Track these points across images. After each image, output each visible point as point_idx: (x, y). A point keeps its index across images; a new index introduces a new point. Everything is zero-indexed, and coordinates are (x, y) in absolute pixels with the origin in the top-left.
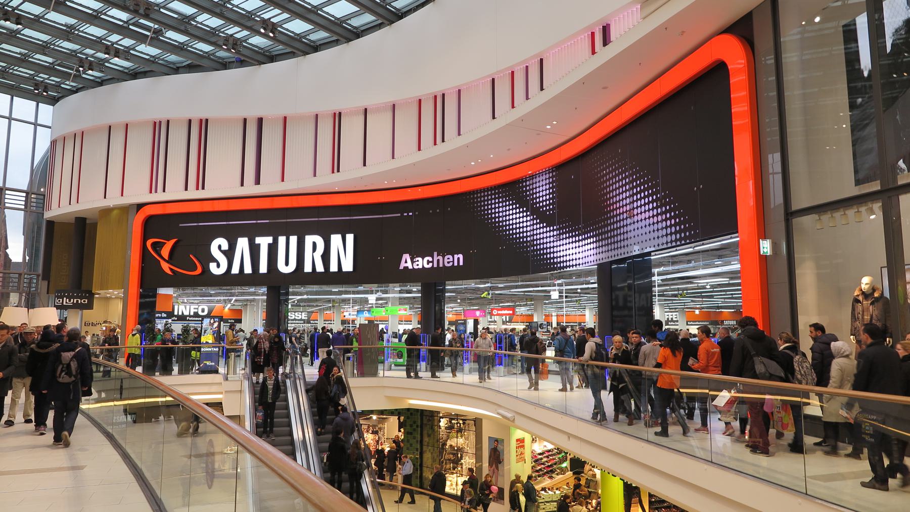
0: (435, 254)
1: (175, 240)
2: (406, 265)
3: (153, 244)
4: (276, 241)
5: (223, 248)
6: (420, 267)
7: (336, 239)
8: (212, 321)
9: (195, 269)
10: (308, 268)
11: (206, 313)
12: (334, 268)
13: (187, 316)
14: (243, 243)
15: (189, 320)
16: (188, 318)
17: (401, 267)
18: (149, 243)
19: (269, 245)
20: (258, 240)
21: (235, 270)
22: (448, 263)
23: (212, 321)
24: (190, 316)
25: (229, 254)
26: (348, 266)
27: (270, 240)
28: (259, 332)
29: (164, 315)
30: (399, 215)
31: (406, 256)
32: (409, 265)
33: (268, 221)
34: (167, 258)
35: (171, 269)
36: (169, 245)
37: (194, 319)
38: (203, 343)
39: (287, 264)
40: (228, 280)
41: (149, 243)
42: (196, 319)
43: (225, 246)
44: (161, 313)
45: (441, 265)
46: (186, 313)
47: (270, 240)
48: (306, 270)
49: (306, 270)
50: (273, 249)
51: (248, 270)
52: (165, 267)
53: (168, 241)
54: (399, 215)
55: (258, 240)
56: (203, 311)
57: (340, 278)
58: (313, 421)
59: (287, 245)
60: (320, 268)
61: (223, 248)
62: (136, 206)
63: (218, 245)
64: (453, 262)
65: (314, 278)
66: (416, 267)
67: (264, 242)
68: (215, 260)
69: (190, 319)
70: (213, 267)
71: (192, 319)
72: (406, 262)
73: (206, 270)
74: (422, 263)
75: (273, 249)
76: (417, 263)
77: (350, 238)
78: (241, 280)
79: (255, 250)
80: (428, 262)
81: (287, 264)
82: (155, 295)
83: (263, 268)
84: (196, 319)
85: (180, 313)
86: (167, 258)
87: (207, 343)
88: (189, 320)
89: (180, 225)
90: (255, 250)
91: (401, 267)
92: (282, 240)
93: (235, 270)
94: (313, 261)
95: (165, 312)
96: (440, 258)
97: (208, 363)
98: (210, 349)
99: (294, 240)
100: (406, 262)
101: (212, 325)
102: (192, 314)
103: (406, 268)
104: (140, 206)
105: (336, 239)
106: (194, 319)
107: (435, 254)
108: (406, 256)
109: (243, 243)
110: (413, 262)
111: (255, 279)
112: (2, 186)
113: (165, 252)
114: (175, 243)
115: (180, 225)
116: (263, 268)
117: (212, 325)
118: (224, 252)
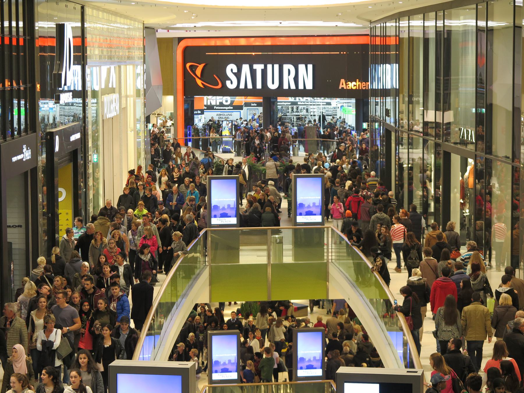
0: (357, 80)
1: (204, 64)
2: (343, 86)
3: (191, 67)
4: (266, 67)
5: (234, 71)
6: (350, 88)
7: (302, 67)
8: (228, 122)
9: (218, 85)
10: (286, 87)
11: (229, 103)
12: (301, 87)
13: (214, 106)
14: (246, 68)
15: (216, 109)
16: (215, 107)
17: (340, 88)
18: (188, 65)
19: (262, 70)
20: (255, 66)
21: (242, 86)
22: (364, 87)
23: (228, 122)
24: (217, 106)
25: (238, 75)
26: (309, 86)
27: (262, 66)
28: (8, 359)
29: (199, 112)
30: (338, 53)
31: (343, 81)
32: (344, 86)
33: (261, 53)
34: (199, 76)
35: (202, 84)
36: (201, 67)
37: (220, 108)
38: (224, 136)
39: (273, 83)
40: (237, 92)
41: (188, 65)
42: (222, 108)
43: (235, 70)
44: (197, 110)
45: (360, 88)
46: (213, 103)
47: (262, 66)
48: (284, 88)
49: (284, 88)
50: (264, 72)
51: (250, 86)
52: (199, 82)
53: (200, 64)
54: (338, 53)
55: (255, 66)
56: (226, 101)
57: (305, 93)
58: (324, 191)
59: (273, 70)
60: (293, 87)
61: (234, 71)
62: (177, 39)
63: (231, 68)
64: (366, 87)
65: (290, 93)
66: (348, 88)
67: (259, 67)
68: (229, 79)
69: (217, 108)
70: (228, 83)
71: (217, 108)
72: (343, 84)
73: (224, 85)
74: (352, 85)
75: (264, 72)
76: (348, 85)
77: (310, 67)
78: (245, 93)
79: (253, 73)
80: (354, 86)
81: (273, 83)
82: (193, 98)
83: (259, 86)
84: (222, 108)
85: (209, 104)
86: (199, 76)
87: (226, 135)
88: (216, 109)
89: (207, 54)
90: (253, 73)
91: (340, 88)
92: (269, 66)
93: (242, 86)
94: (288, 82)
95: (200, 110)
96: (360, 83)
97: (227, 147)
98: (227, 139)
99: (276, 67)
100: (343, 84)
101: (228, 125)
102: (218, 104)
103: (343, 88)
104: (180, 39)
105: (302, 67)
106: (220, 108)
107: (357, 80)
108: (343, 81)
109: (246, 68)
110: (346, 85)
111: (254, 92)
112: (376, 387)
113: (198, 72)
114: (204, 66)
115: (207, 54)
116: (259, 86)
117: (228, 125)
118: (234, 74)
